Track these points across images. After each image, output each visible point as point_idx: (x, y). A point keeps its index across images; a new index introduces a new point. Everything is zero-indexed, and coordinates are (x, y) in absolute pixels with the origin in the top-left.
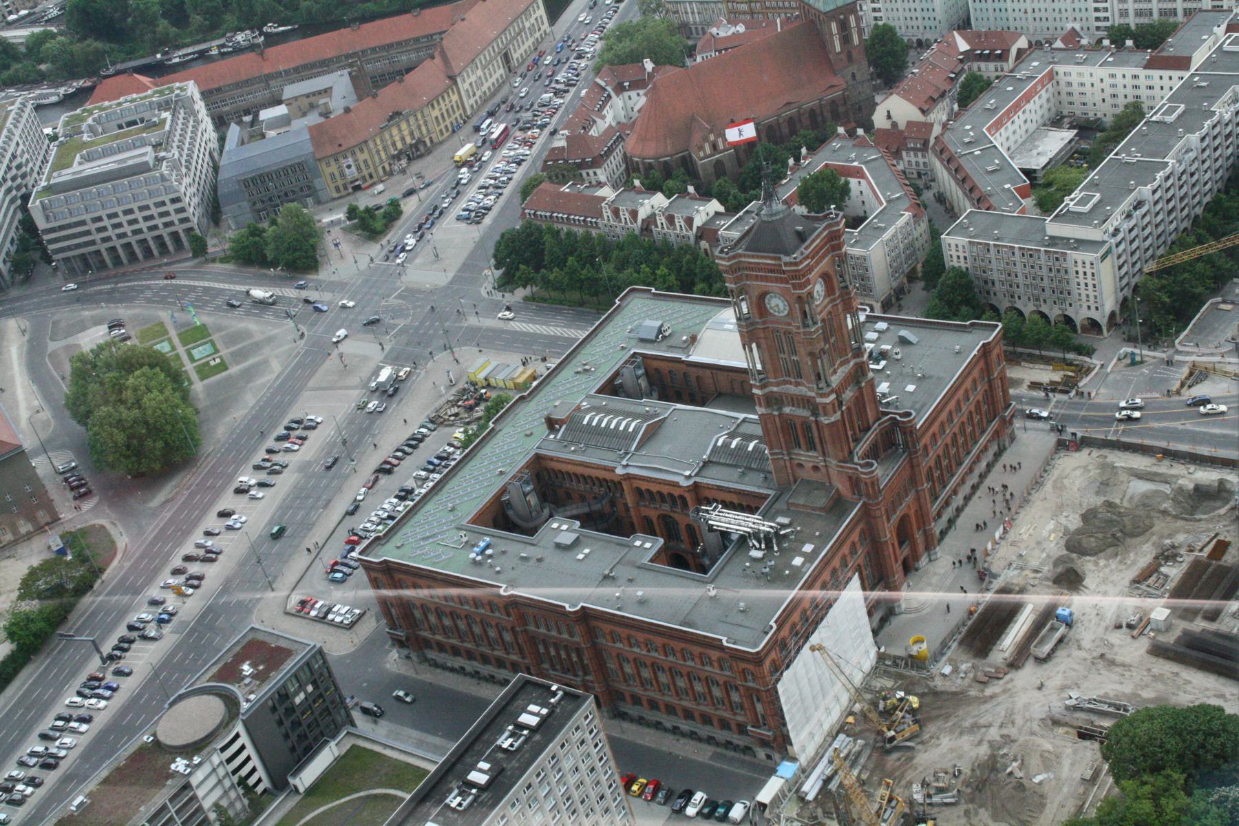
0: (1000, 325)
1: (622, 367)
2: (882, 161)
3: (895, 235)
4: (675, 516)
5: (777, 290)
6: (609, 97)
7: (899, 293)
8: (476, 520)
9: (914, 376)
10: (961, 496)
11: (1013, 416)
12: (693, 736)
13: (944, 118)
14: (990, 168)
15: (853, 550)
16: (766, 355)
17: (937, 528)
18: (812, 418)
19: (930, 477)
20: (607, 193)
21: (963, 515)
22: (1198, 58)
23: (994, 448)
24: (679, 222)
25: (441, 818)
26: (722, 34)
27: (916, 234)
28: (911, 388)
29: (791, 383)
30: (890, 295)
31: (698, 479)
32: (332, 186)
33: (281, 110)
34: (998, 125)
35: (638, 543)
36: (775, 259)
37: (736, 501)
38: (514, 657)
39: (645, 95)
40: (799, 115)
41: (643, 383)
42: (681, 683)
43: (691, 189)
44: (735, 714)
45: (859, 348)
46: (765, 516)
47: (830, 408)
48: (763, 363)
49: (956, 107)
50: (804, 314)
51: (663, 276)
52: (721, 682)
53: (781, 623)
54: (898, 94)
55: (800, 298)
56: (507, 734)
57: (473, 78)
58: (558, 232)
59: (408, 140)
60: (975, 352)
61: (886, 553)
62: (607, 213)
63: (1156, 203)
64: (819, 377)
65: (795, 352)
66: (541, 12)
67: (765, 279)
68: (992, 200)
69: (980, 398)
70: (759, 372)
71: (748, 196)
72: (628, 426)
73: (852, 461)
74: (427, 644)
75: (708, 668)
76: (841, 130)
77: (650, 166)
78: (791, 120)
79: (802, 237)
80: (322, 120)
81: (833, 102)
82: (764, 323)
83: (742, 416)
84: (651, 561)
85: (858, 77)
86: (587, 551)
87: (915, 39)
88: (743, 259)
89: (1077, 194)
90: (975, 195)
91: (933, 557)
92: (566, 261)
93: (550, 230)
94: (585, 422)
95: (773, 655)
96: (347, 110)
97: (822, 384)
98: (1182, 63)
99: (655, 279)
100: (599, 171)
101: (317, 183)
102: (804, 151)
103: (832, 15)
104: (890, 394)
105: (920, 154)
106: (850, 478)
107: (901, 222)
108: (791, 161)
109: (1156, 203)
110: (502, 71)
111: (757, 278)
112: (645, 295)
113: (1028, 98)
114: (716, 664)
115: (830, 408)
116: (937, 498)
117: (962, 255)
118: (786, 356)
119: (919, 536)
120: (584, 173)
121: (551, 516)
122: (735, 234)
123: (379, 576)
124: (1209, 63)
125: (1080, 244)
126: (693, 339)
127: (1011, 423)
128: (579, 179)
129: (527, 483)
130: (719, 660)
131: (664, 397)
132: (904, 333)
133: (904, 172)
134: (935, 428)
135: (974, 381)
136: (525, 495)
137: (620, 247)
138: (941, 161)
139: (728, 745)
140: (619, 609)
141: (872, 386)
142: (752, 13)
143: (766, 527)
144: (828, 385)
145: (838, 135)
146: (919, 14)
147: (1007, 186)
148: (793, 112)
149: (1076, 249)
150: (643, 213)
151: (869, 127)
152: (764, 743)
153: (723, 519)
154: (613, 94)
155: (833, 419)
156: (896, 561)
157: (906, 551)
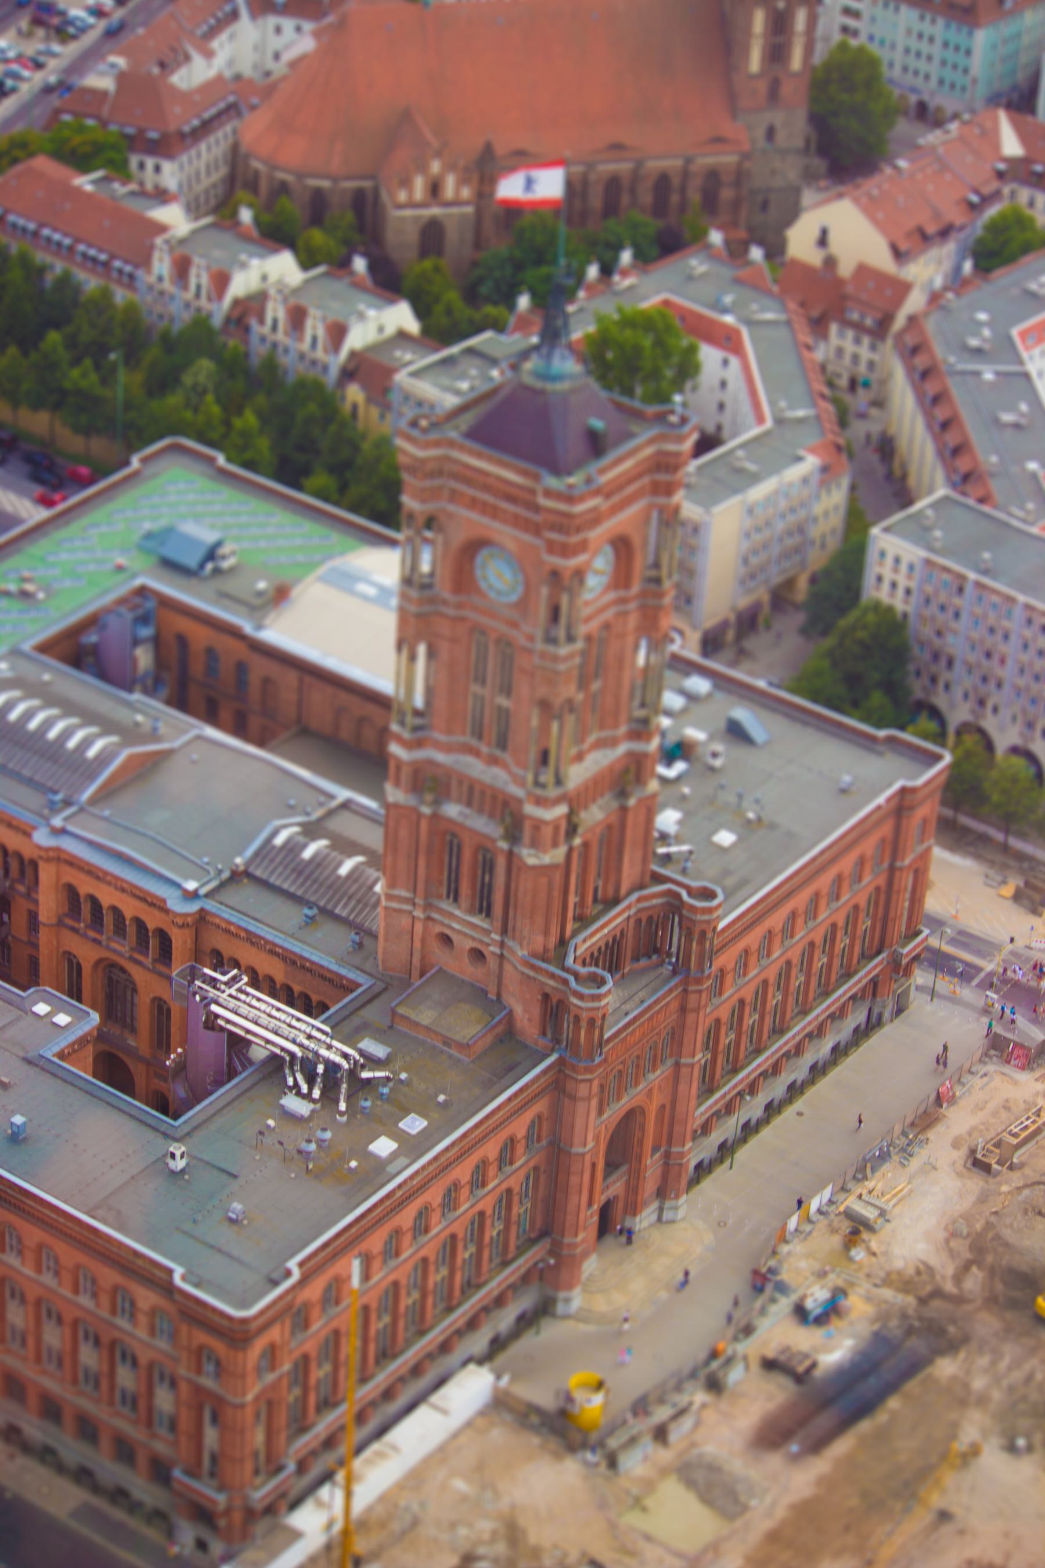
0: (948, 758)
1: (107, 611)
2: (783, 333)
3: (768, 500)
4: (137, 974)
5: (511, 545)
6: (234, 15)
9: (738, 810)
10: (761, 1099)
11: (916, 958)
12: (46, 1455)
13: (938, 282)
14: (1007, 417)
15: (506, 1156)
17: (696, 1153)
18: (503, 845)
19: (712, 1040)
21: (753, 1142)
23: (857, 1017)
24: (315, 327)
27: (818, 509)
28: (725, 838)
29: (477, 753)
30: (724, 625)
31: (211, 905)
35: (41, 1008)
36: (525, 473)
37: (280, 978)
39: (317, 34)
40: (636, 176)
41: (144, 658)
42: (53, 1337)
43: (360, 264)
44: (154, 1436)
45: (645, 722)
46: (340, 1028)
47: (547, 832)
48: (430, 692)
49: (968, 266)
50: (555, 614)
51: (246, 435)
53: (311, 1269)
54: (856, 201)
55: (555, 575)
58: (42, 270)
60: (881, 800)
61: (574, 1180)
62: (162, 265)
64: (544, 758)
65: (507, 690)
67: (494, 513)
68: (995, 486)
69: (862, 900)
70: (417, 713)
71: (477, 316)
72: (86, 743)
73: (560, 960)
75: (122, 1322)
76: (716, 237)
77: (283, 188)
78: (613, 184)
81: (713, 176)
82: (460, 606)
83: (343, 794)
84: (61, 1055)
85: (781, 137)
87: (913, 99)
88: (456, 454)
90: (963, 464)
91: (667, 1215)
92: (39, 335)
93: (24, 260)
95: (274, 1334)
99: (225, 436)
100: (167, 167)
102: (626, 257)
104: (678, 839)
105: (866, 341)
106: (546, 997)
107: (794, 473)
111: (473, 504)
114: (143, 1319)
115: (547, 832)
116: (711, 1091)
117: (902, 582)
118: (485, 692)
119: (652, 1165)
120: (134, 160)
126: (281, 595)
127: (908, 972)
128: (119, 169)
130: (153, 1312)
131: (180, 702)
132: (742, 714)
133: (823, 368)
134: (753, 939)
135: (861, 862)
137: (169, 343)
138: (910, 369)
139: (119, 1495)
141: (650, 809)
144: (559, 782)
145: (708, 247)
148: (624, 167)
150: (241, 285)
151: (775, 250)
153: (244, 1009)
155: (547, 859)
156: (590, 1204)
157: (616, 1187)
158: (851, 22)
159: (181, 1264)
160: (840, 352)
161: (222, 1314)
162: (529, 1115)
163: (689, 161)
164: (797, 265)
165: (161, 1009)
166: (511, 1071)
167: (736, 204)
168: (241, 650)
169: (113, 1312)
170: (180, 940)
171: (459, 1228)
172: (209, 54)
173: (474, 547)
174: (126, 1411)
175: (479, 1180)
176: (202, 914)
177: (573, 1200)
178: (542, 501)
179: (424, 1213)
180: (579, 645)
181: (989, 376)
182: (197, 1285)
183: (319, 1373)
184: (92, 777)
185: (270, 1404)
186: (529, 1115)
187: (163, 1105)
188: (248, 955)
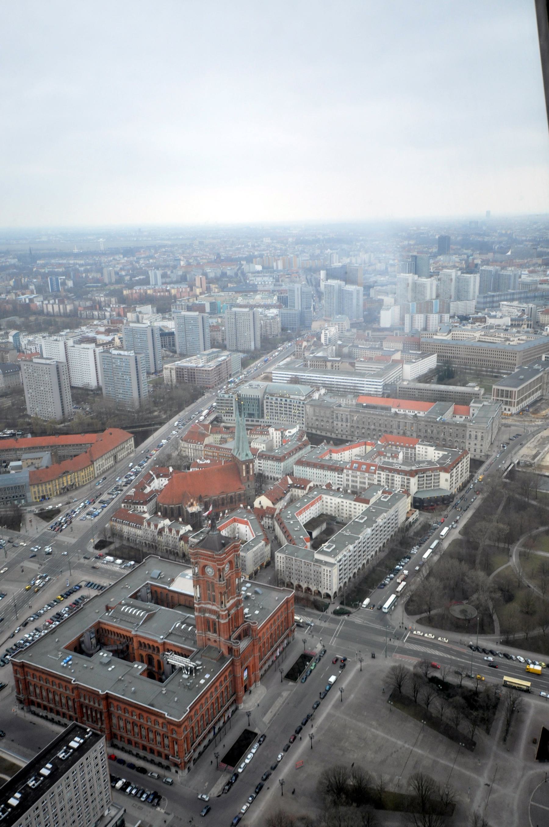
2: (256, 520)
4: (154, 656)
6: (154, 479)
7: (256, 572)
8: (67, 648)
9: (259, 607)
14: (296, 529)
16: (202, 591)
18: (217, 620)
25: (23, 791)
27: (266, 550)
29: (210, 604)
30: (252, 574)
31: (165, 640)
32: (34, 496)
33: (19, 463)
37: (180, 652)
38: (72, 713)
39: (168, 480)
40: (227, 497)
41: (149, 596)
44: (165, 750)
45: (239, 593)
46: (192, 660)
47: (224, 616)
48: (200, 594)
50: (220, 576)
52: (161, 734)
55: (219, 570)
56: (63, 751)
57: (101, 463)
59: (69, 483)
62: (145, 524)
63: (355, 552)
66: (235, 454)
68: (296, 541)
69: (283, 619)
75: (157, 727)
79: (224, 545)
83: (188, 615)
84: (141, 674)
85: (250, 486)
86: (113, 667)
89: (327, 544)
94: (122, 609)
95: (186, 723)
97: (223, 606)
100: (145, 507)
101: (28, 495)
103: (244, 462)
104: (249, 614)
106: (229, 647)
107: (260, 545)
108: (221, 515)
109: (355, 552)
110: (113, 462)
111: (203, 559)
112: (156, 559)
121: (100, 649)
122: (196, 541)
123: (19, 669)
125: (326, 563)
126: (173, 580)
127: (294, 631)
129: (93, 633)
130: (162, 723)
132: (257, 589)
134: (264, 630)
135: (282, 612)
136: (91, 639)
138: (278, 523)
140: (123, 695)
141: (243, 609)
143: (192, 665)
144: (225, 606)
145: (240, 507)
147: (301, 537)
150: (160, 526)
151: (252, 507)
154: (155, 478)
158: (260, 465)
159: (166, 712)
160: (266, 522)
161: (176, 721)
162: (228, 671)
163: (235, 493)
164: (256, 508)
165: (159, 662)
166: (223, 663)
167: (245, 499)
168: (167, 592)
169: (155, 725)
170: (161, 648)
171: (218, 695)
172: (150, 486)
173: (204, 567)
174: (159, 745)
175: (221, 684)
176: (164, 643)
177: (239, 686)
178: (215, 556)
179: (212, 693)
180: (225, 581)
181: (292, 522)
182: (170, 716)
183: (196, 729)
184: (142, 620)
185: (187, 738)
186: (228, 671)
187: (161, 681)
188: (174, 649)
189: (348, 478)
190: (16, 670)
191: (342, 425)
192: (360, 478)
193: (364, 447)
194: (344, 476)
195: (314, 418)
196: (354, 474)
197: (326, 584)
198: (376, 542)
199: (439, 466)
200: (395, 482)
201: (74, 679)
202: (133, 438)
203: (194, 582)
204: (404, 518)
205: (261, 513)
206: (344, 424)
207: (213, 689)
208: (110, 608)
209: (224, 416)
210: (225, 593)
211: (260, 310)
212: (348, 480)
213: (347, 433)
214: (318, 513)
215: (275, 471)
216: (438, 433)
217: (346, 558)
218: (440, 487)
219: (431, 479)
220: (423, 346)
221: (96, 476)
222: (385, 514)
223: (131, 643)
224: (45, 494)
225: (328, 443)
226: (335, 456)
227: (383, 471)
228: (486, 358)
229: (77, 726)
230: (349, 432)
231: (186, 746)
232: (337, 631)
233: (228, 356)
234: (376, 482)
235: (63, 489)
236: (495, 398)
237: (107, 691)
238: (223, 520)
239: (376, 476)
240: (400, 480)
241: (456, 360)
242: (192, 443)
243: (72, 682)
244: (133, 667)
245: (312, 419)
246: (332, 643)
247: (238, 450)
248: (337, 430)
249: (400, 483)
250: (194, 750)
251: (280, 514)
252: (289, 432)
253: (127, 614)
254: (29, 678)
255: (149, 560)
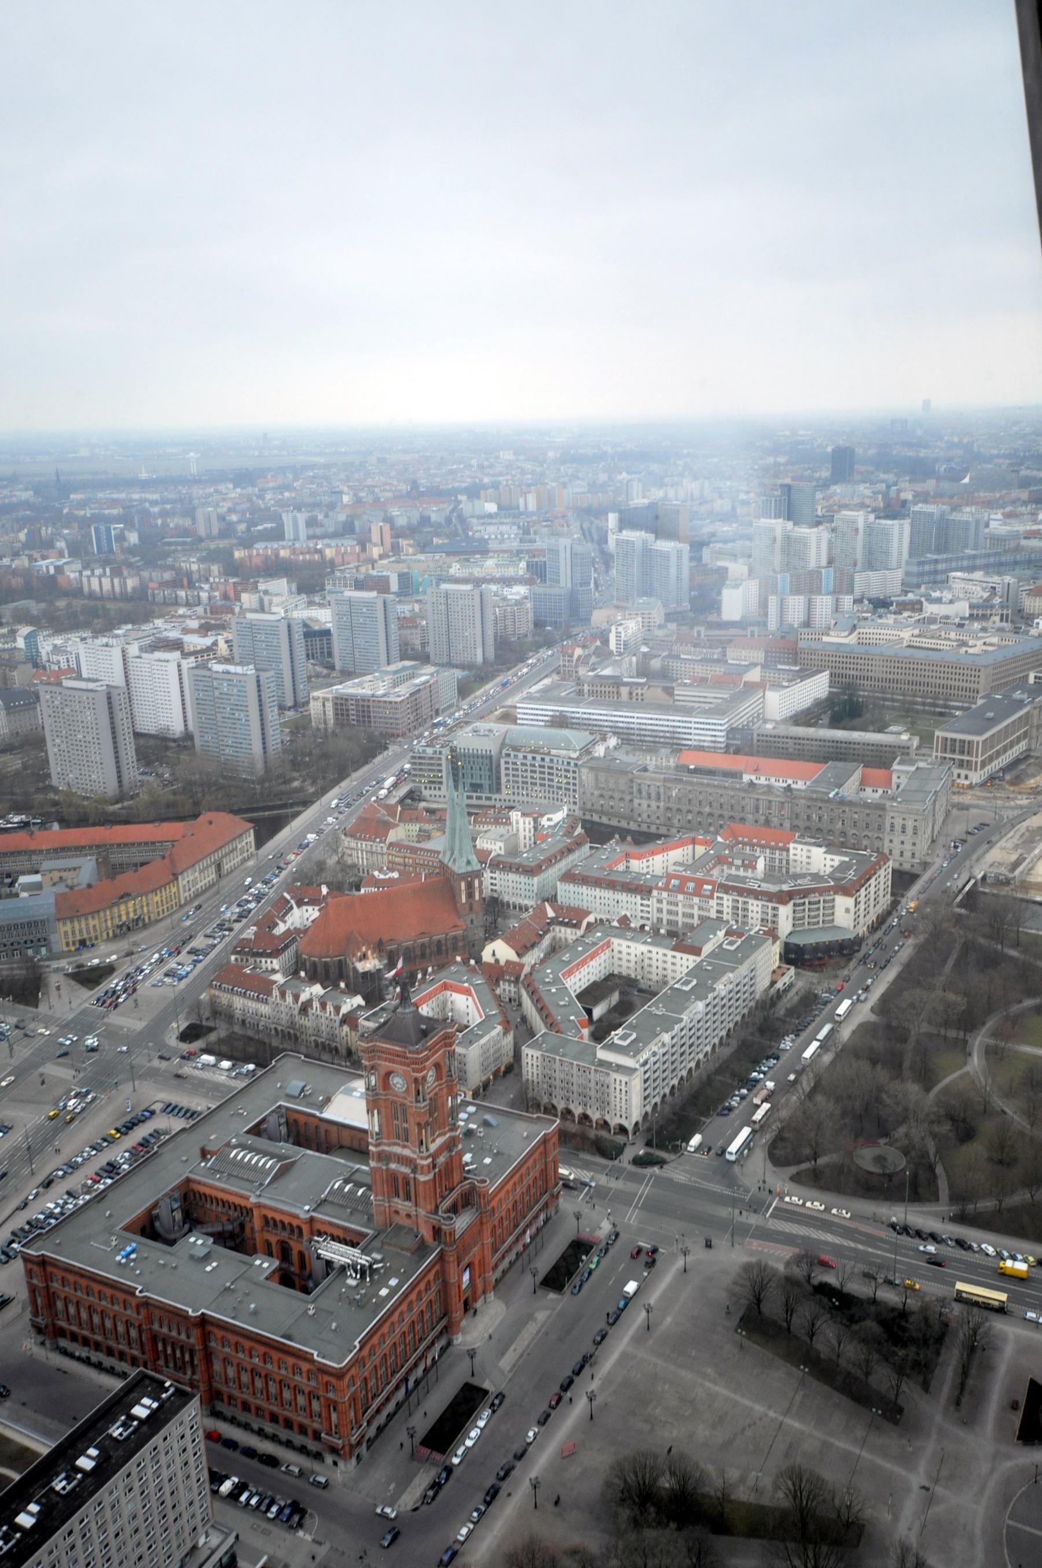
2: (486, 986)
4: (292, 1243)
7: (486, 1085)
8: (127, 1228)
9: (491, 1150)
14: (562, 1003)
16: (384, 1120)
18: (412, 1175)
20: (279, 978)
22: (707, 949)
25: (44, 1501)
26: (382, 876)
27: (504, 1043)
29: (398, 1145)
30: (478, 1088)
31: (314, 1214)
33: (37, 878)
34: (570, 973)
37: (342, 1236)
39: (319, 910)
40: (430, 942)
41: (284, 1130)
43: (342, 985)
44: (313, 1421)
45: (454, 1124)
46: (365, 1251)
47: (426, 1168)
48: (380, 1126)
50: (418, 1093)
55: (416, 1080)
56: (119, 1423)
59: (132, 915)
62: (276, 993)
63: (673, 1046)
66: (251, 838)
68: (562, 1026)
69: (537, 1174)
74: (61, 1332)
75: (297, 1378)
79: (425, 1034)
80: (67, 890)
83: (358, 1166)
84: (267, 1279)
85: (475, 922)
86: (214, 1264)
89: (620, 1031)
94: (232, 1156)
95: (353, 1371)
96: (89, 886)
97: (424, 1148)
98: (696, 951)
100: (275, 961)
103: (463, 877)
104: (472, 1163)
106: (434, 1227)
107: (494, 1033)
108: (420, 976)
109: (673, 1046)
111: (386, 1060)
112: (296, 1061)
113: (592, 957)
121: (190, 1231)
122: (372, 1025)
123: (35, 1268)
124: (713, 954)
125: (619, 1068)
126: (328, 1100)
127: (557, 1197)
129: (176, 1200)
130: (308, 1371)
132: (488, 1117)
134: (502, 1194)
135: (535, 1161)
136: (172, 1211)
138: (528, 992)
140: (233, 1318)
141: (460, 1155)
142: (405, 865)
143: (364, 1260)
144: (427, 1150)
145: (456, 962)
146: (522, 886)
147: (572, 1018)
149: (617, 1071)
150: (304, 997)
151: (479, 960)
152: (334, 1450)
158: (494, 881)
159: (315, 1349)
160: (504, 990)
161: (333, 1368)
162: (433, 1272)
163: (447, 934)
164: (487, 964)
165: (301, 1255)
166: (423, 1257)
167: (464, 946)
168: (317, 1122)
169: (294, 1374)
170: (305, 1229)
171: (415, 1318)
172: (285, 922)
173: (388, 1074)
174: (302, 1413)
175: (420, 1297)
177: (454, 1300)
178: (408, 1055)
179: (402, 1314)
180: (428, 1102)
181: (554, 990)
182: (323, 1358)
184: (269, 1175)
185: (354, 1399)
186: (433, 1272)
187: (306, 1291)
189: (660, 906)
190: (31, 1270)
191: (649, 806)
192: (684, 906)
193: (691, 847)
194: (652, 902)
195: (597, 793)
196: (672, 899)
197: (618, 1108)
198: (713, 1027)
199: (832, 883)
200: (750, 914)
201: (140, 1288)
202: (252, 831)
203: (368, 1103)
204: (767, 983)
205: (495, 973)
206: (654, 804)
207: (404, 1307)
208: (209, 1152)
209: (426, 788)
210: (427, 1124)
211: (494, 588)
212: (660, 910)
213: (658, 822)
214: (603, 972)
215: (523, 892)
216: (832, 821)
217: (657, 1057)
218: (836, 923)
219: (819, 909)
220: (803, 656)
221: (183, 902)
222: (731, 975)
223: (248, 1219)
224: (85, 936)
225: (623, 839)
226: (636, 865)
227: (727, 893)
228: (922, 680)
229: (146, 1376)
230: (662, 819)
231: (352, 1414)
232: (640, 1197)
233: (432, 675)
234: (713, 914)
235: (120, 927)
236: (939, 754)
237: (203, 1310)
238: (423, 986)
239: (713, 903)
240: (759, 909)
241: (865, 682)
242: (364, 840)
243: (137, 1293)
244: (252, 1265)
245: (592, 794)
246: (630, 1219)
247: (452, 854)
248: (640, 815)
249: (759, 916)
250: (369, 1423)
251: (531, 974)
252: (549, 820)
253: (240, 1165)
254: (55, 1285)
255: (283, 1061)
